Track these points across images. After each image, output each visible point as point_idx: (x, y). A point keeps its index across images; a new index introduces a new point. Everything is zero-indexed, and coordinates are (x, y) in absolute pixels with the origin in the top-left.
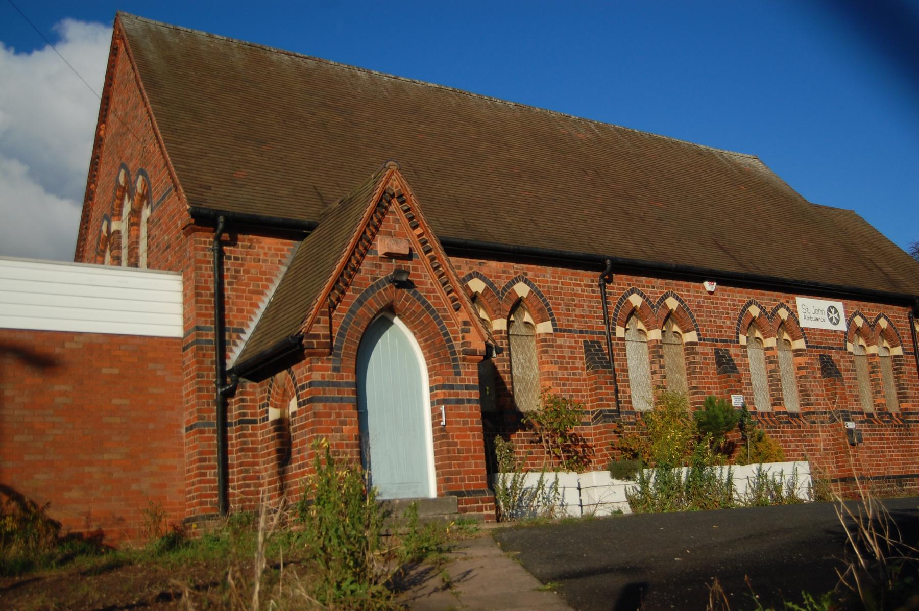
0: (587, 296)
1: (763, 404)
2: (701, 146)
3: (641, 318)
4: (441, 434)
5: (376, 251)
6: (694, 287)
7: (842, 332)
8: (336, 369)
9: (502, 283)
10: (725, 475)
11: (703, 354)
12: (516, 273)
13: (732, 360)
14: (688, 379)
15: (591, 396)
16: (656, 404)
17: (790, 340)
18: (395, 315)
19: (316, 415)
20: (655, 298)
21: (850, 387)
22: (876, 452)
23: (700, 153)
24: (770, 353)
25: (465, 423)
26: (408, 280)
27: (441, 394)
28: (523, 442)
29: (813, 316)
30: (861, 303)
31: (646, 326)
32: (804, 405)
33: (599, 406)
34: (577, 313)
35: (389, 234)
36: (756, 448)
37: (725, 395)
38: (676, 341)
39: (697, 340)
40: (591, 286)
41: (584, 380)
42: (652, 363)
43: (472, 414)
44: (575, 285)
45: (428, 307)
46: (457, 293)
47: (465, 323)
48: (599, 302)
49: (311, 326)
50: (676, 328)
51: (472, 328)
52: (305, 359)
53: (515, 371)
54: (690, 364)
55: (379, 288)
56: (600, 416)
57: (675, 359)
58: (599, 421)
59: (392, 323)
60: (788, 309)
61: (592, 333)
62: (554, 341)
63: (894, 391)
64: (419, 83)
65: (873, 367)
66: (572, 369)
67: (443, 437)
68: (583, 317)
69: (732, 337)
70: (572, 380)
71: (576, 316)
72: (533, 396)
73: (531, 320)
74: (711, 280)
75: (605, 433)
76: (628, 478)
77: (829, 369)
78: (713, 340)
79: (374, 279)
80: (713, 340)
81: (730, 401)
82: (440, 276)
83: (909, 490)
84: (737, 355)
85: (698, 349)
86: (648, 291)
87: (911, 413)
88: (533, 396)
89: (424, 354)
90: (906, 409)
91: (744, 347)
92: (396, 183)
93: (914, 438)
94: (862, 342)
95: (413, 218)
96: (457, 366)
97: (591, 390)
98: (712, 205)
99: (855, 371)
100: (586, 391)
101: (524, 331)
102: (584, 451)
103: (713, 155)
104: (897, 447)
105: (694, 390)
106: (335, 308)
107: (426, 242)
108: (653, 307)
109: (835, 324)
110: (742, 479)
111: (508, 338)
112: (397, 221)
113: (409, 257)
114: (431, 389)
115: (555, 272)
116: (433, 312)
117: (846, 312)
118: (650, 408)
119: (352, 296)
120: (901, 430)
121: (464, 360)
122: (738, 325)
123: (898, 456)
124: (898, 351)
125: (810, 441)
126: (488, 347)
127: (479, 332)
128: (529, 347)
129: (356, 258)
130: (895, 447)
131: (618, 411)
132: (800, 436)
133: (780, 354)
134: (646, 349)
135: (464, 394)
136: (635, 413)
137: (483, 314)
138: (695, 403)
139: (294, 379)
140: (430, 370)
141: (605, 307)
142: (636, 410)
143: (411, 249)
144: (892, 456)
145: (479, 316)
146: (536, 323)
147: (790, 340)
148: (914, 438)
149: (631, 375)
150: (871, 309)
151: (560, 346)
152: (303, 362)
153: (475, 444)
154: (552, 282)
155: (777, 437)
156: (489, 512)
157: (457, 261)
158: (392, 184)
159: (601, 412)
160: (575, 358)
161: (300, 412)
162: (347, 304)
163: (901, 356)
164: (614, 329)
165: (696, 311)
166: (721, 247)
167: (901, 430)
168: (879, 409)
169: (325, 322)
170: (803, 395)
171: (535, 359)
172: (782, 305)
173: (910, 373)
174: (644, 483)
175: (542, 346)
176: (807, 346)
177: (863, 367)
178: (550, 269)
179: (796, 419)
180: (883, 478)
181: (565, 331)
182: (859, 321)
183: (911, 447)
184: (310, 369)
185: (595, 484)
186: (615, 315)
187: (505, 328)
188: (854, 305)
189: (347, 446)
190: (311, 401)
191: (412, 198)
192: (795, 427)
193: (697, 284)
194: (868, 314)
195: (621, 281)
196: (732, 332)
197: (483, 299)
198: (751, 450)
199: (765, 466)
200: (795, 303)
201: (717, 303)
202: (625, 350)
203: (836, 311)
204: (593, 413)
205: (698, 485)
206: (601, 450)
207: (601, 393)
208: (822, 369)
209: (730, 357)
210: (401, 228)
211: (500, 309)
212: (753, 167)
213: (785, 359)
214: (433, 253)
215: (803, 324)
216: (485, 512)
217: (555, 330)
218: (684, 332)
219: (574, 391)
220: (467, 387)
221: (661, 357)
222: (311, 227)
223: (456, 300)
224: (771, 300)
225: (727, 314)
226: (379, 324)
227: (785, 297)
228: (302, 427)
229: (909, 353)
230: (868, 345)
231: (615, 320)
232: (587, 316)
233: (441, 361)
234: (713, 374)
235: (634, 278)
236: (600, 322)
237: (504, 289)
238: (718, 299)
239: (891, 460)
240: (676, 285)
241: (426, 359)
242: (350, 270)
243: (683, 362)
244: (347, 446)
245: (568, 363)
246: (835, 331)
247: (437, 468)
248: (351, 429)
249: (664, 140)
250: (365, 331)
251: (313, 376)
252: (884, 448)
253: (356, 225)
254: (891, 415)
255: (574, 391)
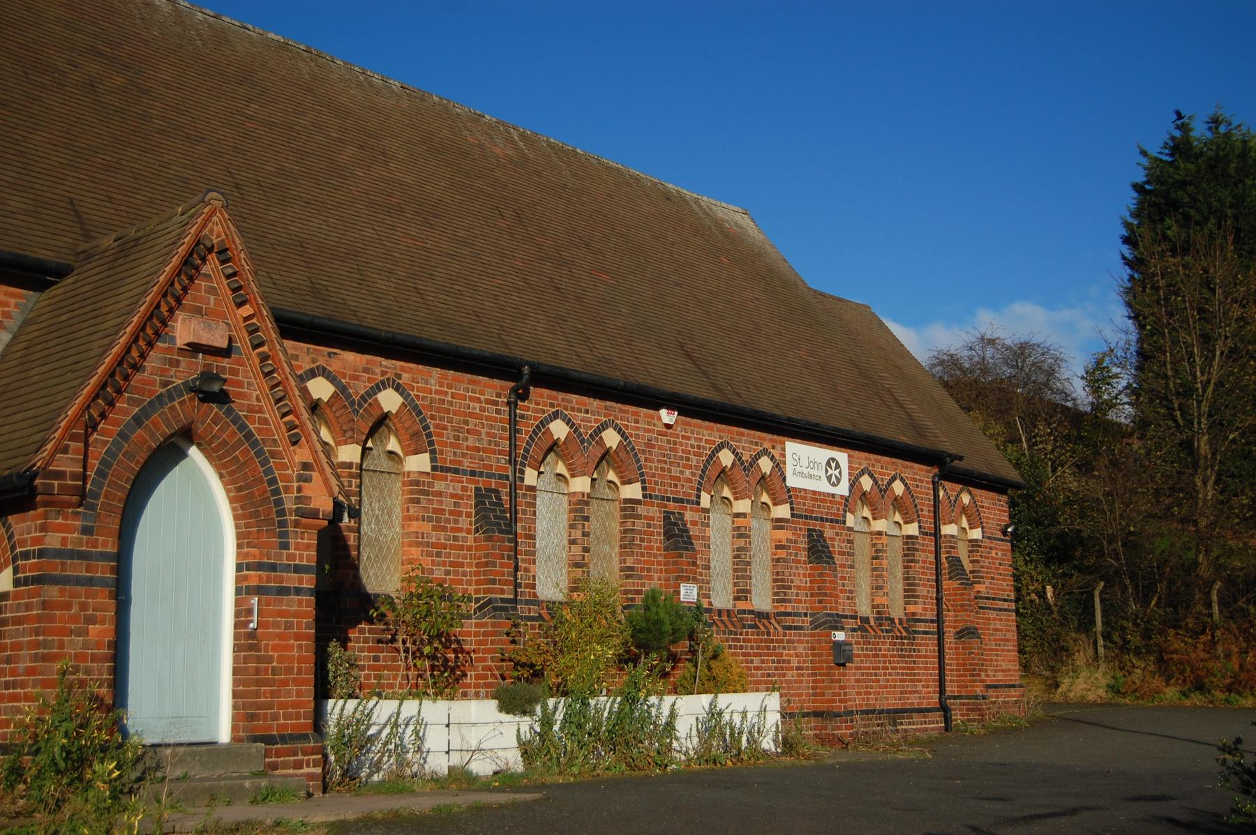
0: (488, 418)
1: (722, 599)
2: (671, 186)
3: (564, 457)
4: (247, 643)
5: (173, 338)
6: (646, 415)
7: (842, 496)
8: (87, 531)
9: (361, 388)
10: (666, 712)
11: (646, 518)
12: (384, 373)
13: (687, 531)
14: (621, 554)
15: (477, 573)
16: (573, 590)
17: (770, 504)
18: (192, 444)
19: (45, 605)
20: (587, 428)
21: (843, 578)
22: (867, 675)
23: (667, 196)
24: (740, 521)
25: (288, 626)
26: (222, 390)
27: (254, 578)
28: (366, 641)
29: (805, 471)
30: (873, 456)
31: (569, 470)
32: (778, 601)
33: (487, 591)
34: (470, 443)
35: (198, 311)
36: (710, 669)
37: (672, 582)
38: (608, 493)
39: (640, 497)
40: (496, 403)
41: (469, 548)
42: (572, 527)
43: (302, 610)
44: (471, 399)
45: (249, 435)
46: (297, 416)
47: (306, 466)
48: (503, 429)
49: (52, 456)
50: (612, 476)
51: (315, 475)
52: (35, 508)
53: (365, 528)
54: (626, 531)
55: (172, 399)
56: (486, 607)
57: (606, 522)
58: (485, 615)
59: (183, 455)
60: (772, 458)
61: (490, 476)
62: (430, 485)
63: (900, 586)
64: (254, 31)
65: (877, 551)
66: (453, 530)
67: (252, 648)
68: (478, 449)
69: (690, 495)
70: (452, 547)
71: (468, 448)
72: (388, 568)
73: (398, 450)
74: (670, 408)
75: (494, 634)
76: (524, 713)
77: (818, 551)
78: (663, 498)
79: (165, 384)
80: (663, 498)
81: (678, 593)
82: (273, 387)
83: (906, 731)
84: (694, 523)
85: (641, 510)
86: (578, 417)
87: (919, 621)
88: (388, 568)
89: (234, 509)
90: (914, 614)
91: (706, 511)
92: (219, 229)
93: (920, 657)
94: (866, 512)
95: (240, 288)
96: (284, 535)
97: (477, 565)
98: (679, 285)
99: (853, 555)
100: (470, 565)
101: (385, 464)
102: (457, 657)
103: (686, 202)
104: (895, 668)
105: (628, 572)
106: (94, 428)
107: (257, 330)
108: (583, 441)
109: (834, 485)
110: (686, 713)
111: (360, 476)
112: (212, 291)
113: (226, 352)
114: (239, 568)
115: (444, 377)
116: (255, 444)
117: (850, 468)
118: (560, 597)
119: (125, 408)
120: (903, 644)
121: (297, 524)
122: (701, 477)
123: (895, 681)
124: (912, 529)
125: (781, 655)
126: (338, 506)
127: (326, 482)
128: (390, 491)
129: (139, 347)
130: (893, 668)
131: (515, 601)
132: (768, 648)
133: (754, 523)
134: (566, 505)
135: (291, 580)
136: (539, 603)
137: (325, 434)
138: (626, 592)
139: (11, 537)
140: (239, 536)
141: (512, 439)
142: (541, 597)
143: (230, 340)
144: (887, 681)
145: (318, 434)
146: (407, 454)
147: (770, 504)
148: (920, 657)
149: (539, 544)
150: (885, 466)
151: (439, 494)
152: (32, 512)
153: (301, 660)
154: (437, 392)
155: (736, 648)
156: (312, 770)
157: (294, 348)
158: (211, 231)
159: (490, 601)
160: (459, 514)
161: (17, 596)
162: (116, 423)
163: (916, 538)
164: (522, 472)
165: (644, 452)
166: (689, 356)
167: (903, 644)
168: (878, 613)
169: (76, 451)
170: (779, 587)
171: (398, 510)
172: (765, 452)
173: (924, 562)
174: (547, 722)
175: (412, 492)
176: (793, 515)
177: (863, 549)
178: (436, 372)
179: (766, 622)
180: (873, 712)
181: (448, 470)
182: (866, 483)
183: (913, 669)
184: (43, 528)
185: (473, 721)
186: (527, 450)
187: (357, 460)
188: (863, 458)
189: (94, 658)
190: (38, 580)
191: (242, 255)
192: (763, 634)
193: (651, 412)
194: (880, 473)
195: (541, 398)
196: (692, 488)
197: (328, 411)
198: (702, 671)
199: (724, 700)
200: (784, 450)
201: (675, 443)
202: (534, 505)
203: (838, 466)
204: (477, 600)
205: (626, 731)
206: (483, 660)
207: (492, 573)
208: (809, 549)
209: (685, 525)
210: (217, 303)
211: (352, 430)
212: (741, 227)
213: (761, 532)
214: (265, 348)
215: (792, 481)
216: (306, 770)
217: (434, 468)
218: (624, 483)
219: (452, 564)
220: (297, 569)
221: (587, 519)
222: (61, 272)
223: (296, 427)
224: (751, 443)
225: (688, 459)
226: (167, 455)
227: (771, 440)
228: (18, 621)
229: (926, 534)
230: (875, 519)
231: (525, 457)
232: (484, 450)
233: (259, 524)
234: (658, 549)
235: (561, 395)
236: (503, 460)
237: (362, 397)
238: (677, 436)
239: (885, 687)
240: (621, 411)
241: (236, 518)
242: (127, 366)
243: (616, 528)
244: (94, 658)
245: (448, 521)
246: (833, 495)
247: (235, 695)
248: (101, 631)
249: (618, 170)
250: (141, 469)
251: (47, 540)
252: (878, 668)
253: (145, 293)
254: (892, 620)
255: (452, 564)
